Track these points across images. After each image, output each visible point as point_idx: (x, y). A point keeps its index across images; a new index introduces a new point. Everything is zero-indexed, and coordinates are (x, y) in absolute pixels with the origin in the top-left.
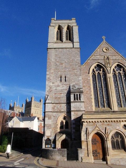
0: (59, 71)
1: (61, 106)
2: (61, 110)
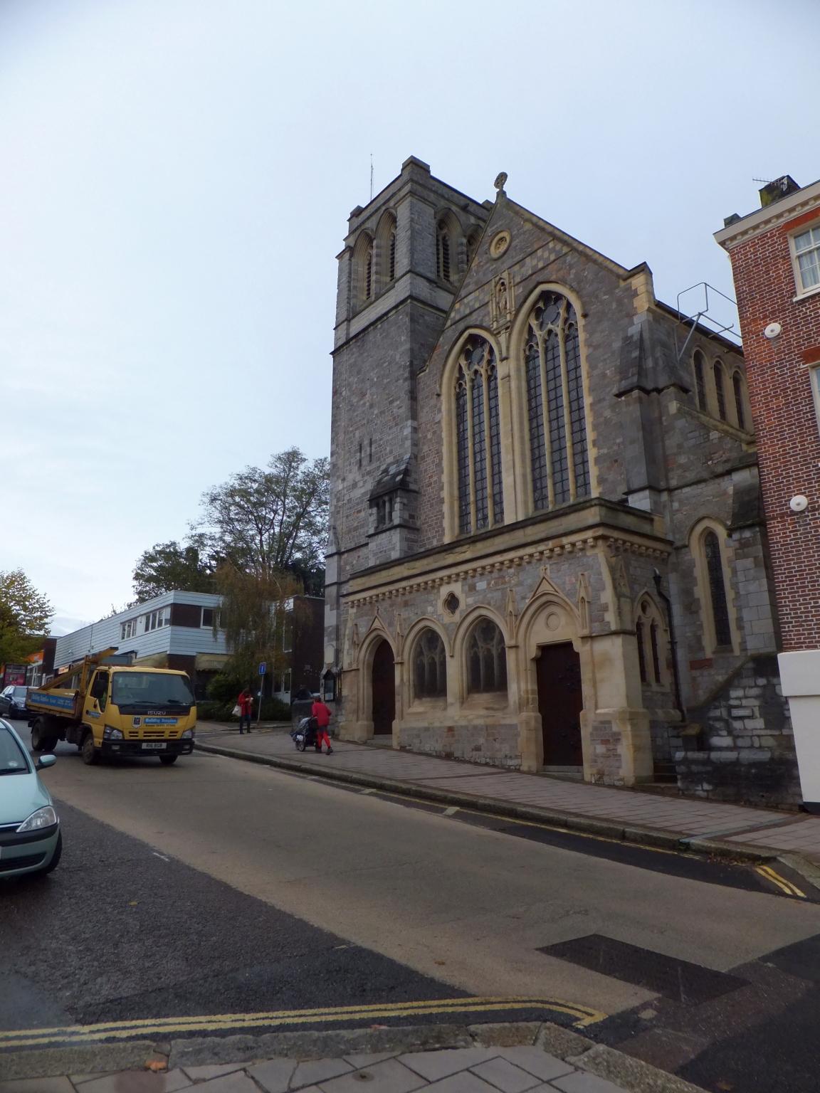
1: (359, 557)
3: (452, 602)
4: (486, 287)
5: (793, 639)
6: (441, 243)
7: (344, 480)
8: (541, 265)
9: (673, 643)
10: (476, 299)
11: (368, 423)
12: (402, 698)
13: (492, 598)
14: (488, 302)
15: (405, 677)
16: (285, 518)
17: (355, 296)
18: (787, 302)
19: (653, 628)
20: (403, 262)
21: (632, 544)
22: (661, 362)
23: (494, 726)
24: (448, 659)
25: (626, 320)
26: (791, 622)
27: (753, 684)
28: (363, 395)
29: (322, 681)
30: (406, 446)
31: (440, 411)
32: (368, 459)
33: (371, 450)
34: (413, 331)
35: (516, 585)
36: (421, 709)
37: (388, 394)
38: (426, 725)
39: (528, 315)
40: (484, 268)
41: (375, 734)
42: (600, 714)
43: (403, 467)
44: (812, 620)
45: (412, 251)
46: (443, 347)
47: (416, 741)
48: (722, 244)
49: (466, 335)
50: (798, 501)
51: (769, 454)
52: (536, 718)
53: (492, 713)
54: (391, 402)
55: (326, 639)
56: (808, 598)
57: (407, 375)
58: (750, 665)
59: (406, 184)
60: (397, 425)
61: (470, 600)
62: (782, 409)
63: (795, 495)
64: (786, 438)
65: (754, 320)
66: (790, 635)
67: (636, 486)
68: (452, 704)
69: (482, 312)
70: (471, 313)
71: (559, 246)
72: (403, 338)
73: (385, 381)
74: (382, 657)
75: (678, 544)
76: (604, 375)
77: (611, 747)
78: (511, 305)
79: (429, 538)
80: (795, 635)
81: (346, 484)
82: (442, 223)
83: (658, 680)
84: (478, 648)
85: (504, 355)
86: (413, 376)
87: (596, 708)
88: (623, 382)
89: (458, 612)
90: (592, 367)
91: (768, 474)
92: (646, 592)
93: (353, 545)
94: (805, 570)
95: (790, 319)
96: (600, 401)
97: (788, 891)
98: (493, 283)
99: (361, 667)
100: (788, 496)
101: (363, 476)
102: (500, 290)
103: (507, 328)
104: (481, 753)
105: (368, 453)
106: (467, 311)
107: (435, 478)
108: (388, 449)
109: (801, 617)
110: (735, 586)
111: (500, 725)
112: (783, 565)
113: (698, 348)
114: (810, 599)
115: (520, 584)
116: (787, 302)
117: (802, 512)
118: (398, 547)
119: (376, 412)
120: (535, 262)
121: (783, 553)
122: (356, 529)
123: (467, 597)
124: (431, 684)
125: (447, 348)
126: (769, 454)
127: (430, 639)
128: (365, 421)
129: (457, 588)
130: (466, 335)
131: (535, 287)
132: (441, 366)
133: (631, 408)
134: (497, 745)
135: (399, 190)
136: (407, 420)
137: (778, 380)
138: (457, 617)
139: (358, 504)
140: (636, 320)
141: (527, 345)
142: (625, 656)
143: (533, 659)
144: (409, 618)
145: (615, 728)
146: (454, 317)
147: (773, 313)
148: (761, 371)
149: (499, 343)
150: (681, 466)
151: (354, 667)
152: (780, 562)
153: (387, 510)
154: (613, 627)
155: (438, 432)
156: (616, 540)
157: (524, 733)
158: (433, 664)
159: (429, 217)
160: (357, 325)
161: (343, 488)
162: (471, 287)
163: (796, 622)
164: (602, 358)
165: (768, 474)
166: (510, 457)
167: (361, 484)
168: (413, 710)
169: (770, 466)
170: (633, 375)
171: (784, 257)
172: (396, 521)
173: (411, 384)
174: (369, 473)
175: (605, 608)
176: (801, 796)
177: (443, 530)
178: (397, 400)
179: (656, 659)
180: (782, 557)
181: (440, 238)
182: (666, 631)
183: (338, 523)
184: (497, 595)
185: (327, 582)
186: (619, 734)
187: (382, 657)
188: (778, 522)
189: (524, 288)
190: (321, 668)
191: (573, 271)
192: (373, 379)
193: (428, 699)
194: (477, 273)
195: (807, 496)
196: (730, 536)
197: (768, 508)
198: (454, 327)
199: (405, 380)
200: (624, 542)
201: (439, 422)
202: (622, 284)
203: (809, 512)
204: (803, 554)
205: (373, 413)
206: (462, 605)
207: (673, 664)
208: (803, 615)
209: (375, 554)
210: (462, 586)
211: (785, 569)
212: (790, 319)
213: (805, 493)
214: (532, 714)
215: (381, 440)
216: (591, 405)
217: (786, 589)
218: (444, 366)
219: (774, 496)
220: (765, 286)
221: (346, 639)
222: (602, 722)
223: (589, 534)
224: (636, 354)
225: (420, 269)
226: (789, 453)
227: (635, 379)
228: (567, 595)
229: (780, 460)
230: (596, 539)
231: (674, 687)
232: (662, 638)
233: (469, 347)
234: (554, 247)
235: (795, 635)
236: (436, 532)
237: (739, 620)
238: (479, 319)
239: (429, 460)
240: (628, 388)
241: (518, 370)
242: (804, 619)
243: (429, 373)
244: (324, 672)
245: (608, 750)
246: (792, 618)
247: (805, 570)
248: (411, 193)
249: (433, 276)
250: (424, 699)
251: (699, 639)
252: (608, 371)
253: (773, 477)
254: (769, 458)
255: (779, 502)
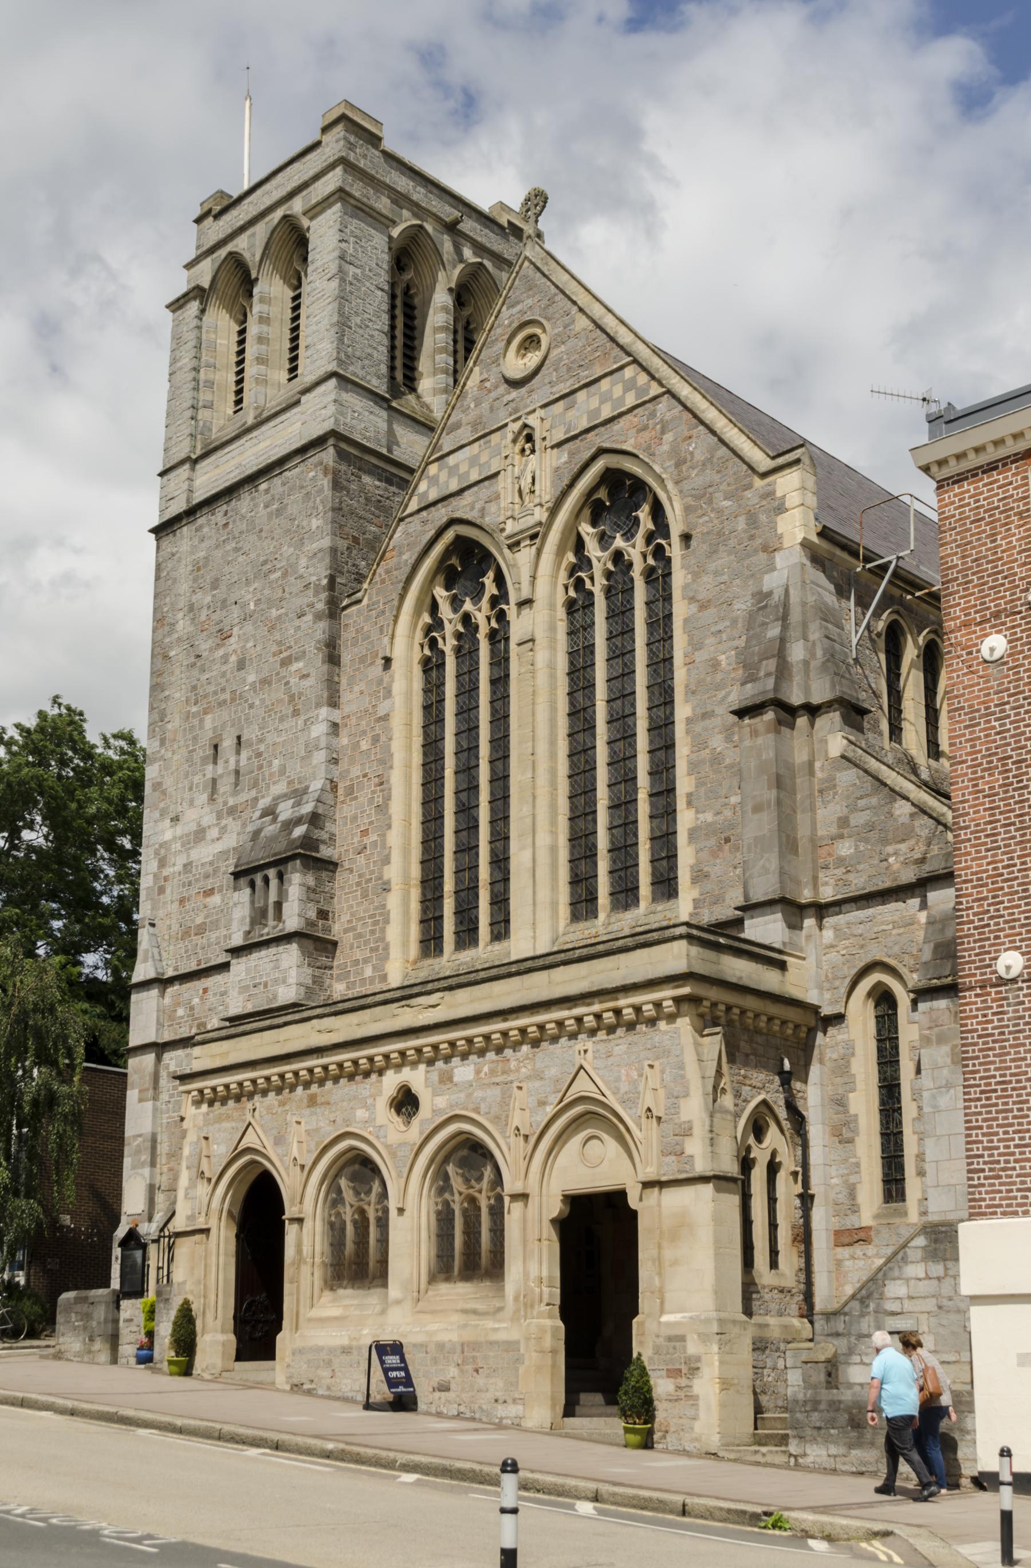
1: (205, 991)
2: (204, 1024)
3: (406, 1102)
4: (495, 438)
5: (984, 1200)
6: (399, 302)
7: (176, 819)
8: (606, 413)
9: (806, 1199)
10: (473, 461)
11: (233, 700)
12: (298, 1288)
13: (483, 1099)
14: (497, 474)
15: (306, 1249)
16: (870, 1414)
17: (209, 406)
18: (1019, 599)
19: (773, 1168)
20: (318, 355)
21: (743, 1012)
22: (819, 653)
23: (475, 1346)
24: (393, 1213)
25: (763, 556)
26: (983, 1170)
27: (922, 1275)
28: (224, 636)
29: (117, 1252)
30: (315, 762)
31: (388, 693)
32: (232, 779)
33: (238, 762)
34: (337, 510)
35: (528, 1078)
36: (335, 1312)
37: (280, 643)
38: (346, 1342)
39: (577, 515)
40: (493, 395)
41: (239, 1358)
42: (668, 1324)
43: (307, 808)
44: (1014, 1169)
45: (343, 325)
46: (401, 554)
47: (325, 1373)
48: (926, 469)
49: (449, 536)
50: (1009, 962)
51: (972, 874)
52: (555, 1329)
53: (473, 1320)
54: (286, 662)
55: (127, 1162)
56: (1010, 1129)
57: (321, 606)
58: (921, 1241)
59: (332, 167)
60: (296, 713)
61: (441, 1102)
62: (997, 794)
63: (1006, 950)
64: (999, 848)
65: (966, 625)
66: (980, 1193)
67: (758, 896)
68: (398, 1302)
69: (483, 492)
70: (460, 492)
71: (643, 378)
72: (315, 523)
73: (274, 613)
74: (259, 1212)
75: (826, 1011)
76: (715, 665)
77: (683, 1382)
78: (546, 491)
79: (356, 962)
80: (987, 1193)
81: (179, 830)
82: (406, 256)
83: (774, 1264)
84: (452, 1194)
85: (525, 594)
86: (334, 611)
87: (662, 1312)
88: (749, 685)
89: (416, 1121)
90: (696, 645)
91: (968, 909)
92: (764, 1102)
93: (193, 967)
94: (1010, 1082)
95: (1022, 631)
96: (706, 715)
97: (883, 1558)
98: (509, 434)
99: (213, 1223)
100: (996, 951)
101: (219, 817)
102: (523, 450)
103: (533, 537)
104: (450, 1395)
105: (232, 765)
106: (454, 486)
107: (374, 837)
108: (276, 762)
109: (998, 1162)
110: (916, 1097)
111: (491, 1343)
112: (978, 1071)
113: (895, 617)
114: (1014, 1132)
115: (538, 1076)
116: (1019, 599)
117: (1014, 981)
118: (292, 980)
119: (251, 678)
120: (594, 403)
121: (980, 1050)
122: (201, 930)
123: (435, 1094)
124: (358, 1264)
125: (409, 557)
126: (972, 874)
127: (360, 1168)
128: (227, 696)
129: (417, 1078)
130: (449, 536)
131: (593, 458)
132: (395, 596)
133: (760, 741)
134: (480, 1380)
135: (316, 177)
136: (318, 705)
137: (995, 741)
138: (415, 1131)
139: (207, 876)
140: (779, 559)
141: (571, 575)
142: (717, 1220)
143: (553, 1221)
144: (317, 1130)
145: (693, 1347)
146: (426, 493)
147: (996, 615)
148: (971, 719)
149: (518, 565)
150: (841, 861)
151: (200, 1223)
152: (974, 1065)
153: (273, 897)
154: (701, 1166)
155: (383, 738)
156: (714, 1005)
157: (531, 1358)
158: (362, 1224)
159: (376, 250)
160: (212, 476)
161: (175, 838)
162: (465, 434)
163: (991, 1170)
164: (713, 629)
165: (968, 909)
166: (526, 809)
167: (214, 833)
168: (314, 1313)
169: (971, 895)
170: (768, 675)
171: (1020, 513)
172: (292, 922)
173: (330, 628)
174: (232, 811)
175: (687, 1132)
176: (911, 1418)
177: (386, 948)
178: (297, 659)
179: (773, 1226)
180: (977, 1058)
181: (399, 292)
182: (795, 1174)
183: (161, 913)
184: (494, 1094)
185: (134, 1041)
186: (698, 1359)
187: (259, 1212)
188: (977, 996)
189: (571, 455)
190: (116, 1221)
191: (669, 437)
192: (246, 604)
193: (349, 1291)
194: (478, 402)
195: (1023, 954)
196: (915, 1003)
197: (964, 970)
198: (424, 513)
199: (318, 617)
200: (729, 1008)
201: (386, 718)
202: (758, 483)
203: (1023, 981)
204: (1009, 1053)
205: (244, 680)
206: (425, 1110)
207: (804, 1237)
208: (1002, 1159)
209: (244, 989)
210: (427, 1072)
211: (981, 1078)
212: (1022, 631)
213: (1020, 947)
214: (548, 1323)
215: (261, 741)
216: (689, 721)
217: (980, 1113)
218: (402, 597)
219: (973, 949)
220: (988, 563)
221: (184, 1164)
222: (670, 1339)
223: (666, 993)
224: (774, 631)
225: (355, 371)
226: (1002, 875)
227: (770, 683)
228: (623, 1102)
229: (986, 885)
230: (677, 1000)
231: (803, 1277)
232: (787, 1189)
233: (454, 561)
234: (633, 380)
235: (987, 1193)
236: (372, 950)
237: (920, 1157)
238: (478, 506)
239: (363, 796)
240: (758, 700)
241: (552, 628)
242: (1002, 1165)
243: (369, 608)
244: (121, 1232)
245: (679, 1388)
246: (985, 1163)
247: (1010, 1082)
248: (341, 194)
249: (382, 389)
250: (341, 1292)
251: (852, 1194)
252: (723, 657)
253: (974, 914)
254: (971, 881)
255: (981, 961)
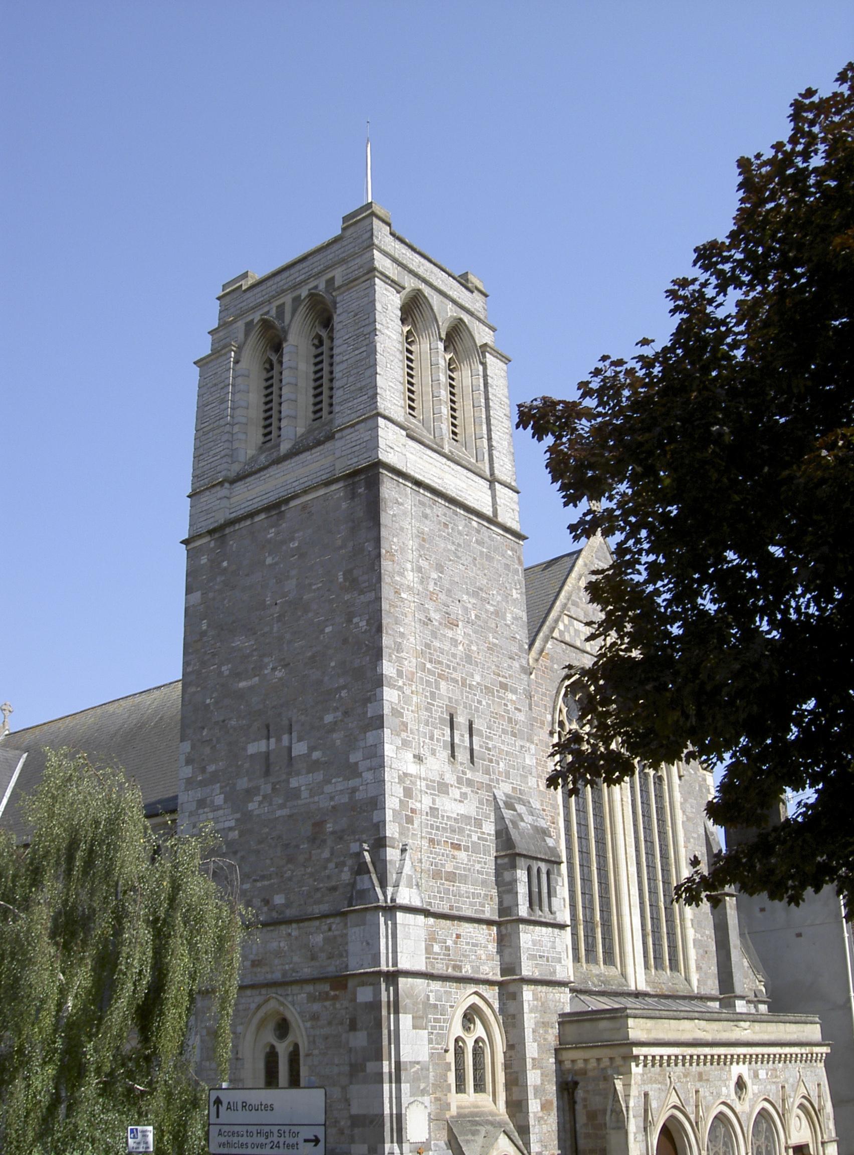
0: (440, 676)
